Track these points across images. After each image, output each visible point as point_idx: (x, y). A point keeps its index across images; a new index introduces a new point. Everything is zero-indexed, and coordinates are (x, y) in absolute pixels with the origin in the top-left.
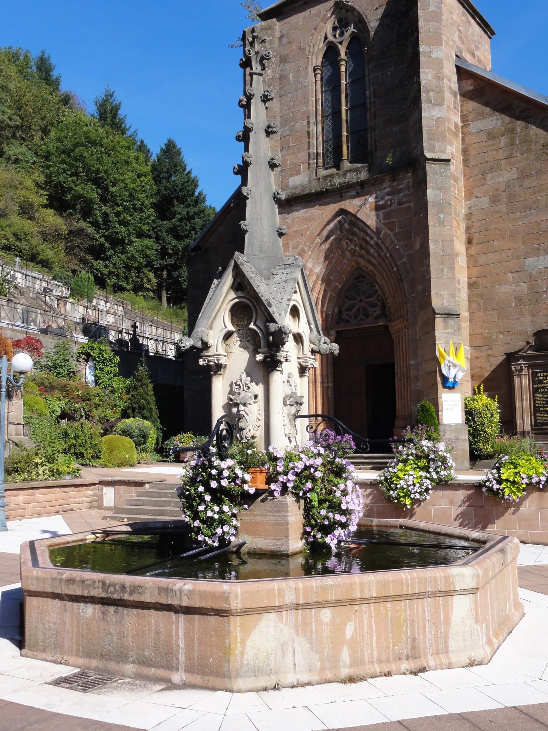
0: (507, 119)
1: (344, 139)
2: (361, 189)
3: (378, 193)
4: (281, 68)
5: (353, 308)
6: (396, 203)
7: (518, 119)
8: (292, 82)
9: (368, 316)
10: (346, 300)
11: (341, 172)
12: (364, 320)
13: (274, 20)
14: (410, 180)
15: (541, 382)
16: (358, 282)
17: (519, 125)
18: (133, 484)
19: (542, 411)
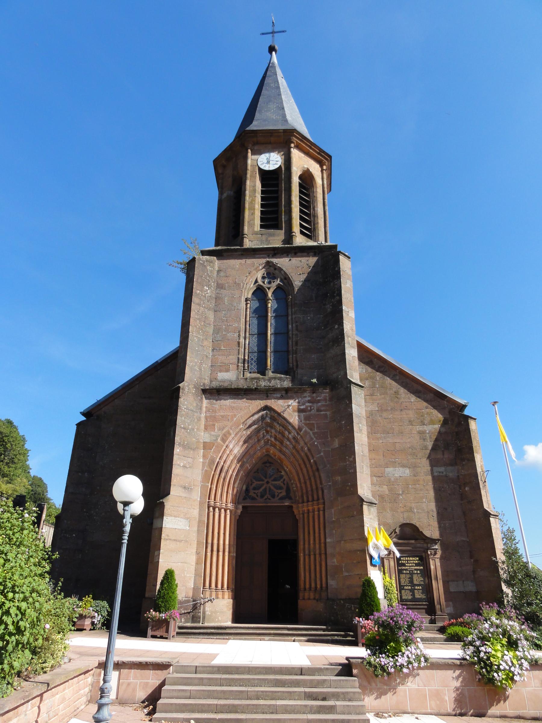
0: (370, 370)
1: (269, 354)
2: (286, 394)
3: (300, 399)
4: (218, 291)
6: (315, 409)
7: (377, 371)
8: (226, 303)
9: (273, 496)
11: (266, 377)
12: (270, 499)
13: (215, 258)
14: (327, 395)
15: (404, 565)
17: (378, 375)
18: (151, 667)
19: (406, 589)
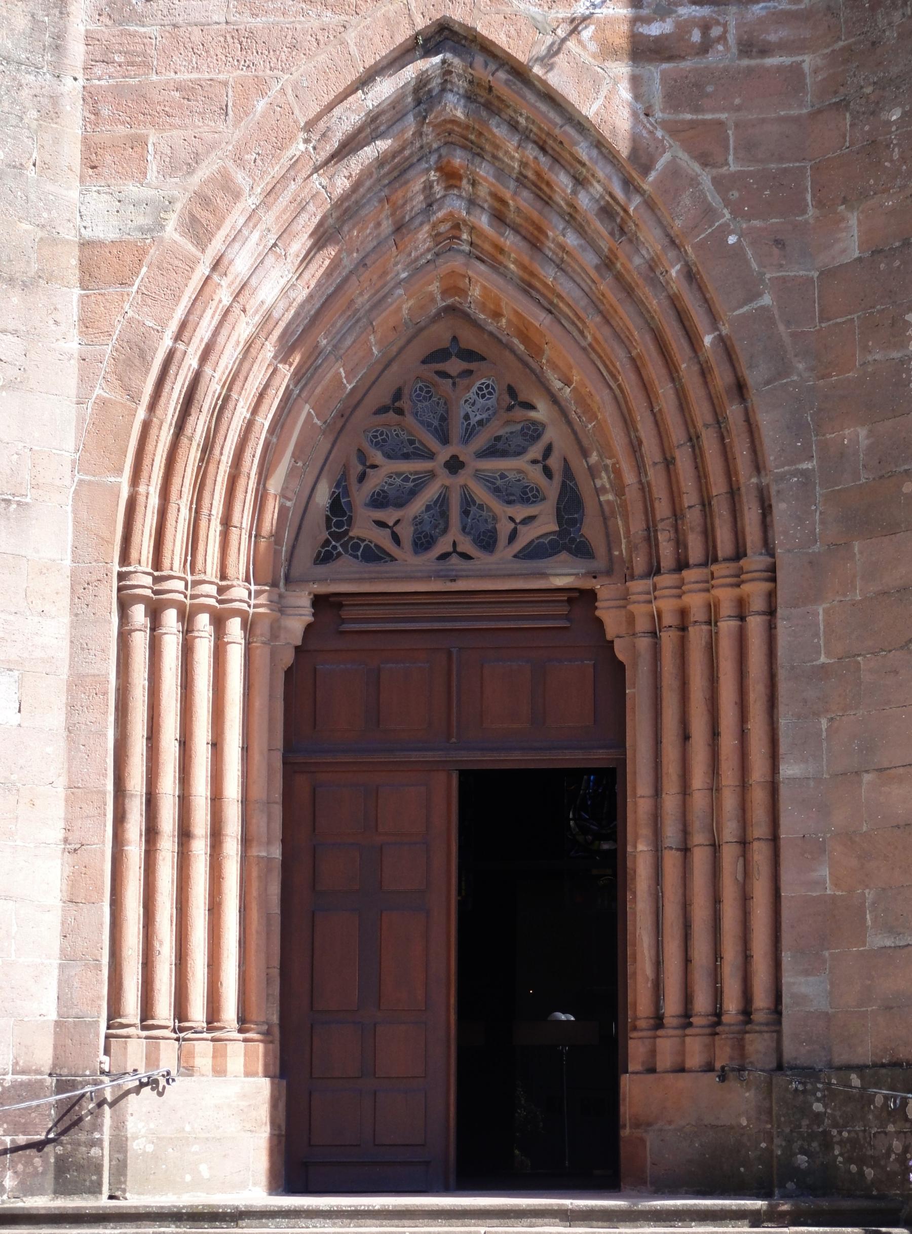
5: (413, 493)
6: (731, 39)
9: (487, 542)
10: (377, 457)
16: (443, 374)
